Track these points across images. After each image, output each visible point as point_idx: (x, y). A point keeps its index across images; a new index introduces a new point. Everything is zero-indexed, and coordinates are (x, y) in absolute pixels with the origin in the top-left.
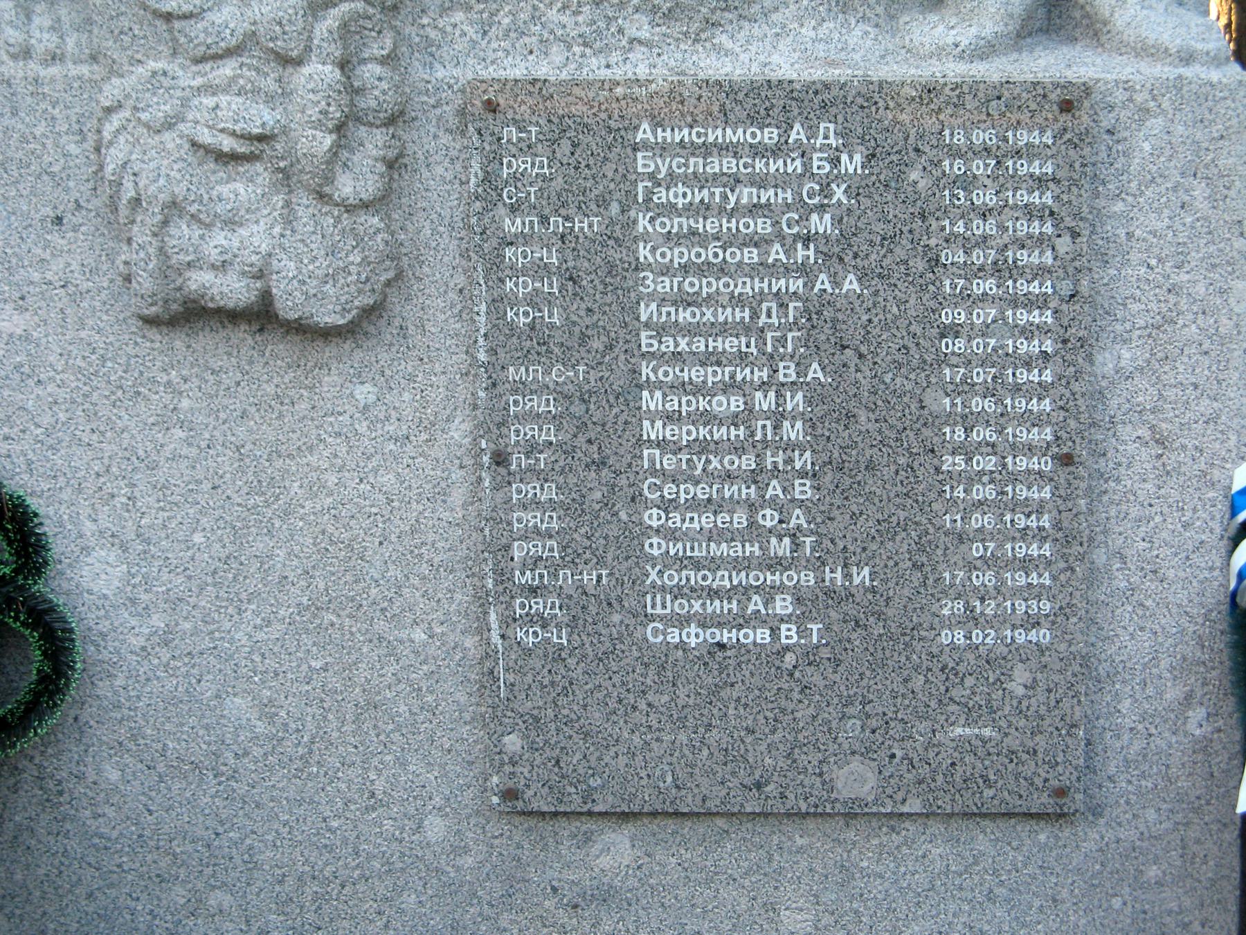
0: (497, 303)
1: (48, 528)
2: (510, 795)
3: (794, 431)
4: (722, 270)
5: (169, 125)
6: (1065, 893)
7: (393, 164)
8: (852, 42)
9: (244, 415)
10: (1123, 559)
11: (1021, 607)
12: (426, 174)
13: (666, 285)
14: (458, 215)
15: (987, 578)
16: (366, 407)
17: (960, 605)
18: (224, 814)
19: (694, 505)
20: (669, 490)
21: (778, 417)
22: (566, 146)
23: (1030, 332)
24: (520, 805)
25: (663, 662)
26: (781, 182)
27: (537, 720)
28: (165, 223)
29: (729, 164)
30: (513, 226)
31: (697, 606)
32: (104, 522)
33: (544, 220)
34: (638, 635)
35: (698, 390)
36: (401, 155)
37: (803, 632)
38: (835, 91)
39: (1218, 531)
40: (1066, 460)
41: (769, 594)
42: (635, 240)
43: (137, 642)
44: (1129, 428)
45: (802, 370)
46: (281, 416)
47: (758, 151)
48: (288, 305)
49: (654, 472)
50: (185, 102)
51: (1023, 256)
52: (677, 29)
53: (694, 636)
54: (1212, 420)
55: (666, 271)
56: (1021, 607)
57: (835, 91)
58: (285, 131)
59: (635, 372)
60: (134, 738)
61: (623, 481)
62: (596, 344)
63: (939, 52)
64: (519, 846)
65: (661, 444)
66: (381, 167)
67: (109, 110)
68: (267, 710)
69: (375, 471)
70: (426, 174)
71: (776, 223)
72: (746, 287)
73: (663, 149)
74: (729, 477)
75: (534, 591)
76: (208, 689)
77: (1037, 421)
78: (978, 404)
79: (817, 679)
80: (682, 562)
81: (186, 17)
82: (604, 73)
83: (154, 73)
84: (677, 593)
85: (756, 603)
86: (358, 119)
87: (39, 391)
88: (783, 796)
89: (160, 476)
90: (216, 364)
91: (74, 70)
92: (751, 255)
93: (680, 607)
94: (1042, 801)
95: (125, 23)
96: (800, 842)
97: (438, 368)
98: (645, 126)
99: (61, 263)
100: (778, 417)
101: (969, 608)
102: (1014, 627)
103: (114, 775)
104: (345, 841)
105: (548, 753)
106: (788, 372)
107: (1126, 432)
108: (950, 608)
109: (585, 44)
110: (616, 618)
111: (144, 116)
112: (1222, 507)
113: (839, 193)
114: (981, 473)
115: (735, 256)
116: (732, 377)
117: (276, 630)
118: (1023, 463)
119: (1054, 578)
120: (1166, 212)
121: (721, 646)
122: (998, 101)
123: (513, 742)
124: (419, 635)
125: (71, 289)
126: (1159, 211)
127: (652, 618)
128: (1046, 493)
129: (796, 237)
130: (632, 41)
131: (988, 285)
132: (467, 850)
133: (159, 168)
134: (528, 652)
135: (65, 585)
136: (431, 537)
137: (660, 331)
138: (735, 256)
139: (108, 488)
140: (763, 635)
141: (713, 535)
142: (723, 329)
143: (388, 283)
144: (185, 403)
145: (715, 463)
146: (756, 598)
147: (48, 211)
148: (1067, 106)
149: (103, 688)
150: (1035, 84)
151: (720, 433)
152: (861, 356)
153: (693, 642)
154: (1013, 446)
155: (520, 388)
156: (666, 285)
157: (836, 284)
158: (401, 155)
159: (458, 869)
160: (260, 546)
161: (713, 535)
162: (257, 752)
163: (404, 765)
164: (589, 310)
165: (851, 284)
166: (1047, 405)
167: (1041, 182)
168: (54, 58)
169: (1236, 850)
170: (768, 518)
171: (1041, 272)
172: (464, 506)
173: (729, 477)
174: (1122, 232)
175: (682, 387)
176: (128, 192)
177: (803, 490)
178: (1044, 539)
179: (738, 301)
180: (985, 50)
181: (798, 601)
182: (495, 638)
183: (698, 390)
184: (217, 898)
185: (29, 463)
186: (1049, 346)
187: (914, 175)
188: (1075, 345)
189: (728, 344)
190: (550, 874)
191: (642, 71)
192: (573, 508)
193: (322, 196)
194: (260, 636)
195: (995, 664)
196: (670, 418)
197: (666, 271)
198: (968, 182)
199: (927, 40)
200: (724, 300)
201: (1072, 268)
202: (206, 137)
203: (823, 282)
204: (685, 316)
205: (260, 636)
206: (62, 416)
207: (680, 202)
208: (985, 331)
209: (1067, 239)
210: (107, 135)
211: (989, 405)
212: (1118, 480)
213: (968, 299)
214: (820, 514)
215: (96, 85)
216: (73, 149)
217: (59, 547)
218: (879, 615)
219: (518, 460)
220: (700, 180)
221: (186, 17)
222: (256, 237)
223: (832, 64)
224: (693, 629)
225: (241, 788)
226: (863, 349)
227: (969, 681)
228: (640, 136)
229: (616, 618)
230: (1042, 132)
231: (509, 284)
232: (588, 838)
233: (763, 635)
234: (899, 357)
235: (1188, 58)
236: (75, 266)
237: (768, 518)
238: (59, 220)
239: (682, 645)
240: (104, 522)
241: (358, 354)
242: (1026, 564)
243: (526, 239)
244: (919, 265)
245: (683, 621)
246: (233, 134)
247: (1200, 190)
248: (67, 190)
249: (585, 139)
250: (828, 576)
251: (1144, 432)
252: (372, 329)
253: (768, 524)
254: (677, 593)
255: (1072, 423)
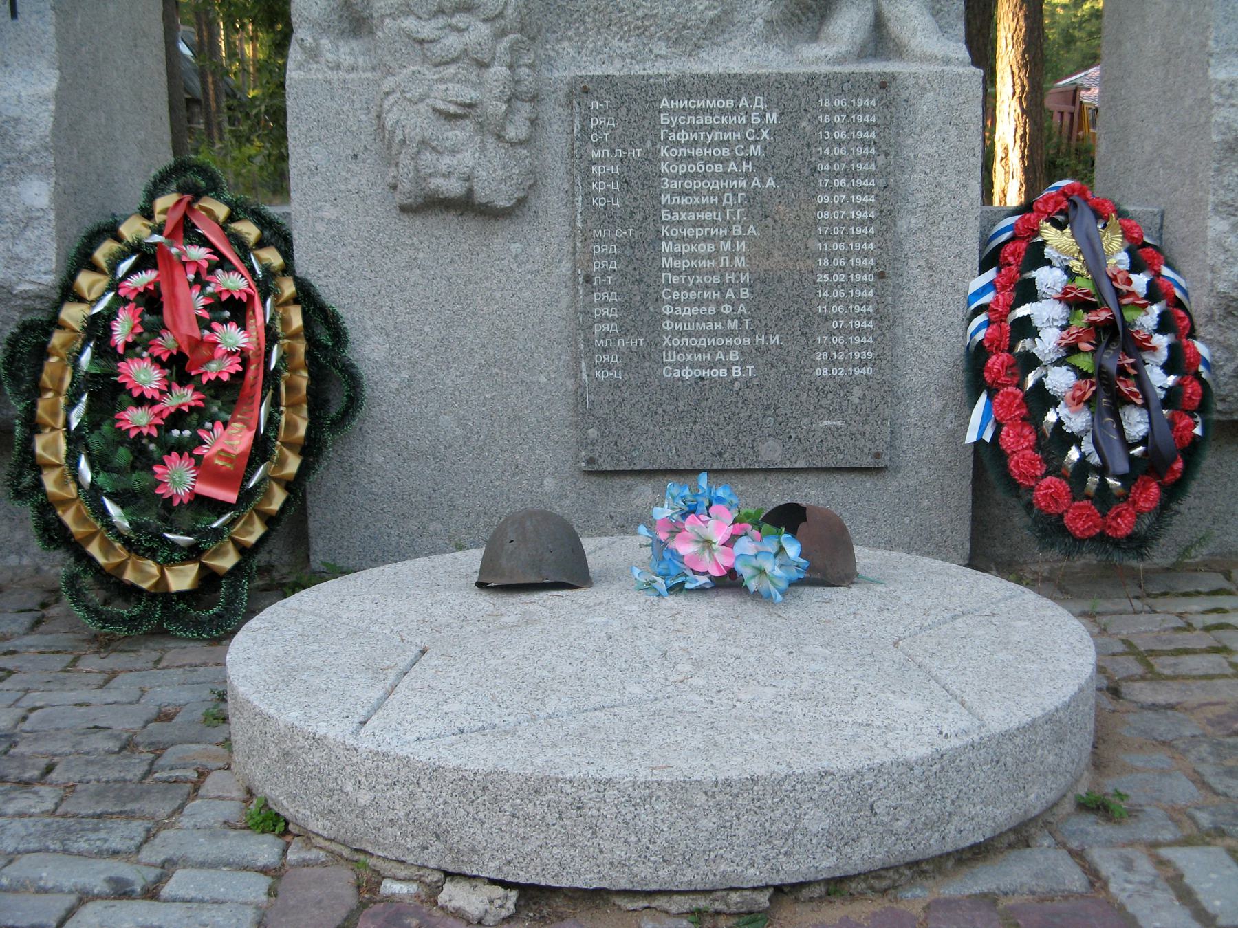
0: (588, 196)
1: (347, 325)
2: (591, 461)
3: (740, 262)
4: (704, 176)
5: (421, 99)
6: (880, 516)
7: (533, 122)
8: (770, 57)
9: (452, 261)
10: (911, 332)
11: (857, 355)
12: (549, 129)
13: (675, 185)
14: (566, 151)
15: (840, 340)
16: (516, 256)
17: (825, 355)
18: (438, 479)
19: (688, 302)
20: (675, 295)
21: (732, 254)
22: (624, 110)
23: (863, 207)
24: (596, 468)
25: (672, 389)
26: (735, 128)
27: (605, 420)
28: (419, 152)
29: (708, 120)
30: (596, 154)
31: (689, 357)
32: (377, 321)
33: (612, 151)
34: (658, 373)
35: (691, 240)
36: (537, 118)
37: (744, 370)
38: (763, 79)
39: (961, 315)
40: (881, 275)
41: (727, 349)
42: (659, 161)
43: (394, 386)
44: (915, 261)
45: (745, 228)
46: (471, 261)
47: (723, 112)
48: (481, 196)
49: (668, 285)
50: (430, 87)
51: (860, 166)
52: (680, 49)
53: (687, 373)
54: (959, 256)
55: (675, 177)
56: (857, 355)
57: (763, 79)
58: (482, 103)
59: (659, 231)
60: (391, 439)
61: (651, 290)
62: (639, 217)
63: (817, 61)
64: (594, 494)
65: (672, 270)
66: (528, 123)
67: (387, 94)
68: (462, 421)
69: (521, 290)
70: (549, 129)
71: (732, 151)
72: (717, 185)
73: (674, 112)
74: (707, 287)
75: (605, 350)
76: (431, 410)
77: (866, 255)
78: (836, 246)
79: (751, 396)
80: (681, 333)
81: (431, 42)
82: (642, 73)
83: (413, 73)
84: (679, 350)
85: (720, 355)
86: (517, 98)
87: (344, 250)
88: (733, 460)
89: (407, 295)
90: (437, 233)
91: (364, 76)
92: (719, 168)
93: (680, 358)
94: (868, 461)
95: (397, 46)
96: (741, 488)
97: (554, 234)
98: (665, 99)
99: (355, 180)
100: (732, 254)
101: (830, 356)
102: (854, 366)
103: (381, 460)
104: (502, 493)
105: (611, 438)
106: (737, 230)
107: (913, 263)
108: (822, 356)
109: (632, 58)
110: (647, 364)
111: (408, 95)
112: (963, 303)
113: (765, 134)
114: (837, 283)
115: (710, 168)
116: (709, 233)
117: (466, 379)
118: (859, 278)
119: (875, 339)
120: (935, 144)
121: (702, 378)
122: (847, 86)
123: (593, 433)
124: (543, 379)
125: (361, 194)
126: (931, 143)
127: (666, 364)
128: (871, 294)
129: (742, 158)
130: (656, 56)
131: (842, 182)
132: (566, 496)
133: (413, 122)
134: (601, 384)
135: (356, 356)
136: (550, 325)
137: (672, 209)
138: (710, 168)
139: (380, 302)
140: (723, 372)
141: (697, 319)
142: (703, 208)
143: (530, 187)
144: (421, 255)
145: (699, 280)
146: (720, 352)
147: (350, 152)
148: (883, 86)
149: (376, 412)
150: (867, 74)
151: (702, 264)
152: (775, 221)
153: (687, 377)
154: (854, 268)
155: (600, 241)
156: (675, 185)
157: (763, 182)
158: (537, 118)
159: (561, 507)
160: (459, 333)
161: (697, 319)
162: (456, 445)
163: (533, 451)
164: (635, 199)
165: (770, 182)
166: (871, 246)
167: (869, 126)
168: (354, 68)
169: (969, 490)
170: (727, 309)
171: (869, 175)
172: (567, 308)
173: (707, 287)
174: (912, 155)
175: (682, 239)
176: (399, 136)
177: (745, 293)
178: (869, 319)
179: (712, 192)
180: (841, 59)
181: (742, 353)
182: (585, 376)
183: (691, 240)
184: (434, 526)
185: (338, 289)
186: (873, 215)
187: (804, 124)
188: (887, 215)
189: (707, 216)
190: (610, 509)
191: (663, 71)
192: (624, 306)
193: (499, 138)
194: (459, 381)
195: (844, 386)
196: (678, 256)
197: (675, 177)
198: (831, 127)
199: (810, 55)
200: (705, 192)
201: (885, 172)
202: (441, 105)
203: (756, 182)
204: (684, 201)
205: (459, 381)
206: (356, 264)
207: (683, 140)
208: (840, 207)
209: (883, 157)
210: (386, 105)
211: (841, 246)
212: (909, 289)
213: (832, 190)
214: (754, 307)
215: (377, 83)
216: (363, 118)
217: (353, 335)
218: (784, 361)
219: (597, 280)
220: (693, 128)
221: (431, 42)
222: (467, 158)
223: (762, 67)
224: (687, 369)
225: (447, 465)
226: (777, 217)
227: (830, 396)
228: (662, 105)
229: (647, 364)
230: (870, 99)
231: (594, 186)
232: (630, 489)
233: (723, 372)
234: (795, 221)
235: (947, 61)
236: (364, 182)
237: (727, 309)
238: (355, 157)
239: (681, 379)
240: (377, 321)
241: (513, 227)
242: (860, 332)
243: (602, 161)
244: (806, 172)
245: (681, 365)
246: (456, 103)
247: (953, 132)
248: (360, 140)
249: (634, 107)
250: (757, 339)
251: (922, 263)
252: (520, 213)
253: (727, 312)
254: (679, 350)
255: (885, 256)
